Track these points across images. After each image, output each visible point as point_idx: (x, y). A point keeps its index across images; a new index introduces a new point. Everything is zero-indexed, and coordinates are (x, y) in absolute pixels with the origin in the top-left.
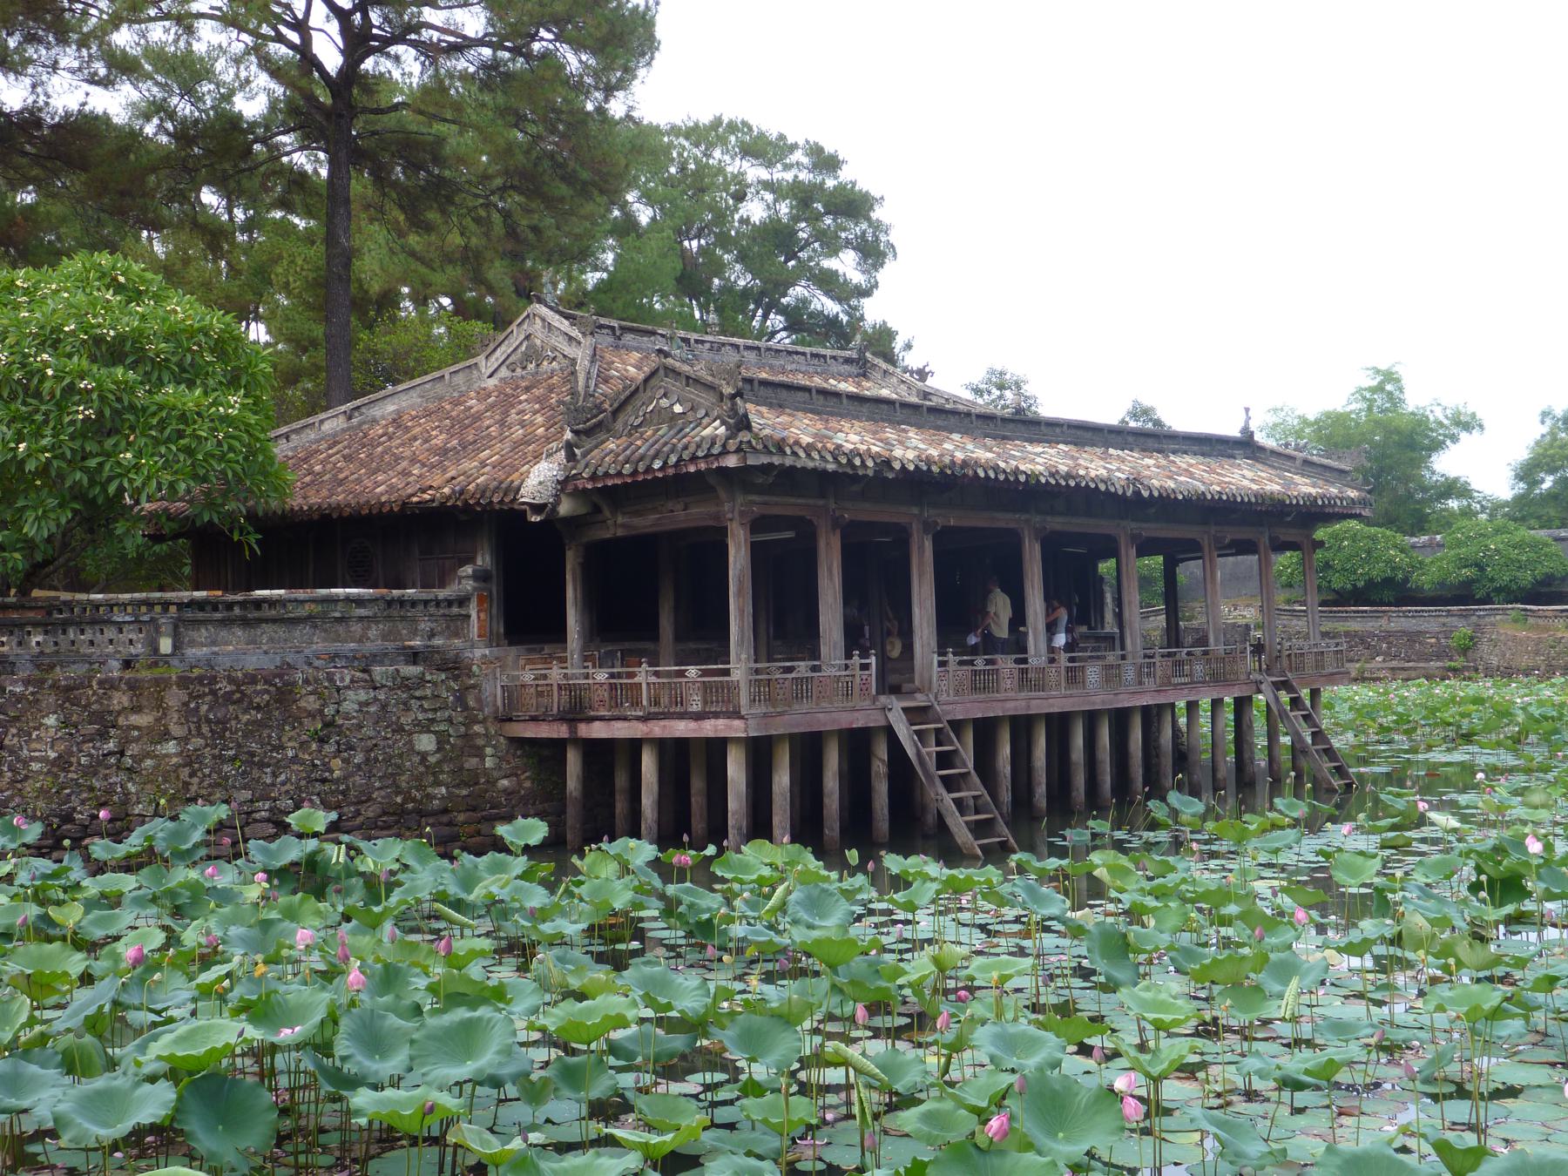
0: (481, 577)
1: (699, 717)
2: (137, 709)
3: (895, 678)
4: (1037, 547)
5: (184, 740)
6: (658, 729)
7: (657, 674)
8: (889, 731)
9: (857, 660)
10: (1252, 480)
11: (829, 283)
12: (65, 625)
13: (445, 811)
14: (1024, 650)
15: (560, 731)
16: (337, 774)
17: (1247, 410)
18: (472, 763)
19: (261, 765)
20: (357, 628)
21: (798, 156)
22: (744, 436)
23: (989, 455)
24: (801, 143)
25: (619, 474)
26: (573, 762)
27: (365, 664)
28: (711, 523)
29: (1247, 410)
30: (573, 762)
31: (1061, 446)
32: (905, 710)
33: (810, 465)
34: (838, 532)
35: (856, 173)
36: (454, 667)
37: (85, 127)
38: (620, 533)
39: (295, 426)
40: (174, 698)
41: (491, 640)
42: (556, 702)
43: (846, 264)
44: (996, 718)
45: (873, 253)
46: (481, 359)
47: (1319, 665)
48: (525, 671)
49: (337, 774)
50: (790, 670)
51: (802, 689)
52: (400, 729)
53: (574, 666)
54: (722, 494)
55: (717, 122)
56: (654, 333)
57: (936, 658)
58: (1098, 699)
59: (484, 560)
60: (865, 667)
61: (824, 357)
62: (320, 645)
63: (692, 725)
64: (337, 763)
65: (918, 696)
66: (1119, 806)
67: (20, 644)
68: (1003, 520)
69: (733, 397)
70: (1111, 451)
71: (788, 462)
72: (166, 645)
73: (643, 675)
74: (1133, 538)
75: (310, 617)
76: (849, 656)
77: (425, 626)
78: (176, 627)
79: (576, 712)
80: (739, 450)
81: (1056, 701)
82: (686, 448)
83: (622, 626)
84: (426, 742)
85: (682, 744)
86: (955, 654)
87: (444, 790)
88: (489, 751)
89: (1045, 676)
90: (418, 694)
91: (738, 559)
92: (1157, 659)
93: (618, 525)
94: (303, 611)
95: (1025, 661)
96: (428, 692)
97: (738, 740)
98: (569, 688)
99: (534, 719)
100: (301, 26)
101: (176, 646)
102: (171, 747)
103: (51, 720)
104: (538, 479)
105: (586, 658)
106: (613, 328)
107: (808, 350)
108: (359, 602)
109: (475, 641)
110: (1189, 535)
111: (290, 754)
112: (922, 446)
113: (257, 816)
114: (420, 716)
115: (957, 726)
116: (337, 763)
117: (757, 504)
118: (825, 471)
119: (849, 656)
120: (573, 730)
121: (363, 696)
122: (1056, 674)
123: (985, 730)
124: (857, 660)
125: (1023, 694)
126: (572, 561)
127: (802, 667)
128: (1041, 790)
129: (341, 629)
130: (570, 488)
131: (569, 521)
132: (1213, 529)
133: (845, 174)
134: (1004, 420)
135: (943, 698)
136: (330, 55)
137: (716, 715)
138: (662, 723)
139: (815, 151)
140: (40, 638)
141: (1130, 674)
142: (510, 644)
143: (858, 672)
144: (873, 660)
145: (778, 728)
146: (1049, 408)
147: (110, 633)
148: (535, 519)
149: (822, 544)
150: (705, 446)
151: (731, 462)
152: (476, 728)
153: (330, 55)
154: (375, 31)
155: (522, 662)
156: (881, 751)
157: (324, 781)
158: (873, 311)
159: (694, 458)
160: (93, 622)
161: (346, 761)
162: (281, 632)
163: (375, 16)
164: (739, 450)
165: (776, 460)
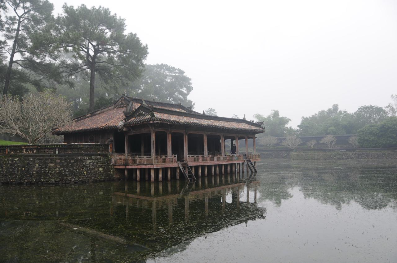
1: (146, 165)
2: (52, 163)
3: (180, 159)
4: (206, 137)
5: (59, 168)
6: (139, 167)
7: (140, 158)
8: (179, 167)
9: (173, 156)
10: (244, 127)
11: (181, 93)
14: (204, 154)
15: (124, 167)
17: (244, 115)
21: (177, 71)
22: (153, 118)
23: (197, 122)
24: (177, 69)
25: (133, 124)
28: (149, 132)
29: (244, 115)
31: (211, 120)
32: (182, 164)
34: (171, 134)
37: (50, 65)
38: (134, 134)
42: (123, 162)
43: (184, 90)
45: (189, 89)
47: (255, 158)
50: (162, 157)
51: (164, 161)
52: (96, 167)
54: (150, 128)
57: (188, 156)
59: (112, 138)
60: (175, 157)
63: (136, 166)
64: (85, 172)
65: (185, 162)
68: (200, 133)
69: (152, 111)
70: (220, 121)
72: (57, 152)
73: (137, 158)
74: (223, 136)
76: (172, 155)
79: (126, 164)
80: (152, 120)
81: (209, 163)
82: (144, 120)
83: (135, 150)
84: (101, 169)
85: (144, 169)
86: (191, 155)
87: (104, 177)
88: (112, 171)
89: (206, 160)
90: (100, 161)
91: (153, 138)
92: (227, 156)
93: (133, 133)
94: (81, 146)
95: (203, 156)
96: (101, 161)
97: (152, 169)
98: (125, 160)
99: (119, 165)
100: (88, 49)
102: (57, 169)
103: (37, 165)
105: (129, 155)
110: (233, 136)
112: (186, 120)
113: (72, 181)
114: (100, 165)
115: (191, 167)
116: (85, 172)
119: (172, 155)
120: (126, 167)
121: (90, 161)
122: (208, 159)
123: (197, 168)
124: (173, 156)
125: (203, 162)
127: (164, 157)
130: (125, 126)
131: (125, 131)
132: (237, 135)
135: (189, 162)
136: (92, 53)
137: (149, 164)
138: (140, 166)
139: (179, 70)
140: (36, 151)
141: (222, 159)
142: (116, 153)
144: (176, 156)
145: (159, 166)
146: (219, 115)
148: (119, 131)
150: (145, 120)
151: (151, 122)
152: (110, 167)
153: (92, 53)
154: (100, 49)
155: (118, 156)
156: (178, 171)
158: (189, 98)
159: (145, 121)
163: (100, 47)
164: (152, 120)
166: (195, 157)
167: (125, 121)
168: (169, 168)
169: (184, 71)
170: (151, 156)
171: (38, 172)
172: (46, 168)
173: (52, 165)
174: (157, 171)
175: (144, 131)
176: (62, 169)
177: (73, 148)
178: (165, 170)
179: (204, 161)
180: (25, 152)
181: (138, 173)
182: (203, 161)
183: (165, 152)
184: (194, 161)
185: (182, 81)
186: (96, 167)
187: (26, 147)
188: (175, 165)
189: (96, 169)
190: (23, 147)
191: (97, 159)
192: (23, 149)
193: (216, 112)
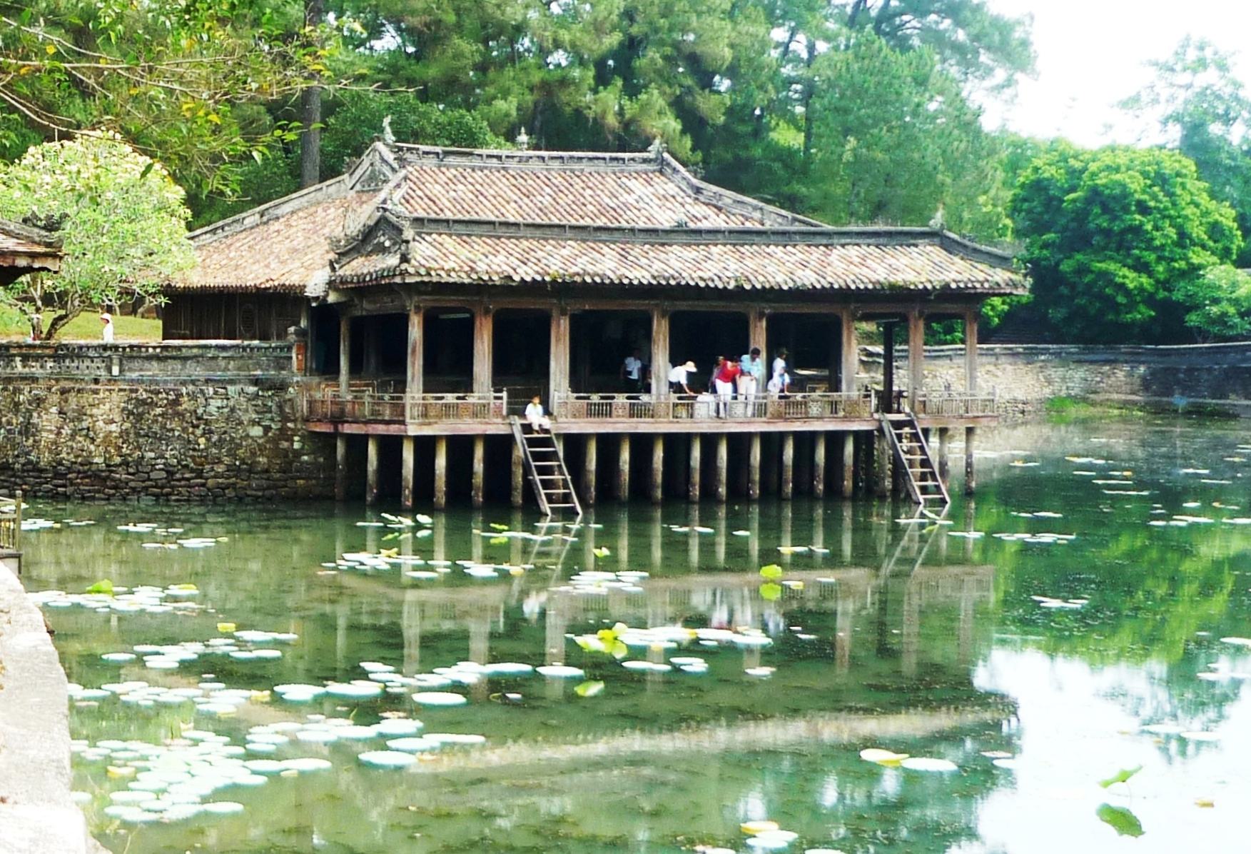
0: (301, 333)
12: (64, 357)
13: (267, 471)
16: (202, 447)
18: (285, 444)
19: (160, 439)
20: (223, 363)
27: (224, 383)
33: (451, 280)
39: (227, 221)
41: (306, 370)
44: (434, 437)
46: (346, 176)
48: (324, 392)
49: (202, 447)
50: (442, 398)
51: (448, 411)
53: (343, 388)
56: (471, 154)
58: (705, 425)
61: (623, 159)
64: (202, 441)
66: (893, 500)
67: (42, 367)
71: (435, 279)
72: (116, 370)
75: (196, 356)
78: (121, 361)
79: (338, 419)
80: (401, 274)
84: (257, 431)
88: (296, 438)
91: (415, 332)
93: (367, 307)
94: (195, 351)
101: (121, 371)
104: (315, 282)
106: (437, 154)
108: (224, 348)
111: (177, 433)
116: (202, 441)
117: (428, 301)
118: (463, 284)
121: (219, 403)
126: (344, 329)
129: (213, 363)
134: (666, 232)
143: (492, 401)
144: (504, 394)
147: (88, 362)
151: (398, 280)
152: (289, 425)
157: (194, 450)
160: (78, 356)
161: (208, 440)
164: (401, 274)
165: (426, 279)
166: (595, 398)
167: (333, 269)
168: (696, 434)
170: (404, 392)
174: (425, 446)
175: (388, 305)
177: (186, 359)
178: (460, 446)
180: (19, 364)
181: (372, 450)
182: (632, 416)
183: (464, 383)
184: (589, 414)
187: (24, 351)
188: (496, 427)
190: (13, 351)
192: (14, 355)
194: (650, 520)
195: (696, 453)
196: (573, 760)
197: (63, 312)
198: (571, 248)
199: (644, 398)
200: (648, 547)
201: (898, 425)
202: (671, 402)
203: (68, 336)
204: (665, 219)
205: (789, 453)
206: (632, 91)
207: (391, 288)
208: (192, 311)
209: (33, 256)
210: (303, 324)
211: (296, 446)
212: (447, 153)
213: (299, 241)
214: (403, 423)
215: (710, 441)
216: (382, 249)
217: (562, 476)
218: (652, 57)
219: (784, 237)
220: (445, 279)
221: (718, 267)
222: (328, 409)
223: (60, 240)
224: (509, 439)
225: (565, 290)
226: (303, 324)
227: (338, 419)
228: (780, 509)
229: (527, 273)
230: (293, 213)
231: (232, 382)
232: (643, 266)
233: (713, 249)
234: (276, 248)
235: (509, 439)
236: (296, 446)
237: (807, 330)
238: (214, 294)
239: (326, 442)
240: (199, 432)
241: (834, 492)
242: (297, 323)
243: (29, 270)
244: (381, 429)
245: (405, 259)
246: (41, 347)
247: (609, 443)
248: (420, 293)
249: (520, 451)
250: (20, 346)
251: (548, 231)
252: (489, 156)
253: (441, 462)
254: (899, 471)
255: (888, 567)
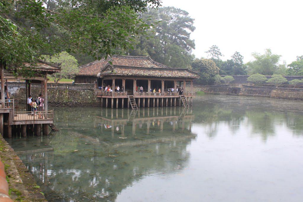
1: (109, 96)
2: (64, 93)
4: (150, 82)
5: (68, 96)
18: (93, 99)
20: (84, 87)
26: (102, 99)
27: (84, 90)
30: (102, 99)
35: (191, 16)
36: (92, 90)
40: (68, 92)
52: (87, 96)
55: (169, 7)
62: (80, 88)
64: (81, 98)
72: (67, 88)
77: (90, 86)
79: (101, 96)
84: (89, 97)
94: (80, 85)
102: (67, 96)
103: (58, 94)
104: (99, 74)
107: (141, 57)
109: (95, 88)
116: (81, 98)
117: (115, 78)
128: (149, 105)
129: (82, 87)
133: (189, 16)
149: (123, 81)
151: (111, 75)
158: (191, 38)
162: (77, 87)
167: (101, 73)
169: (188, 12)
171: (58, 97)
172: (62, 95)
173: (65, 94)
174: (115, 100)
175: (109, 78)
176: (69, 96)
178: (120, 100)
179: (112, 95)
180: (52, 87)
185: (184, 22)
186: (87, 96)
188: (125, 97)
189: (87, 97)
191: (88, 92)
193: (219, 49)
194: (157, 109)
195: (154, 100)
196: (126, 142)
197: (59, 78)
198: (136, 70)
199: (147, 93)
200: (121, 114)
201: (182, 97)
202: (152, 94)
203: (59, 82)
204: (149, 66)
205: (167, 100)
206: (142, 49)
207: (110, 76)
208: (79, 78)
209: (56, 70)
210: (96, 81)
211: (95, 99)
212: (118, 56)
213: (95, 68)
214: (112, 96)
215: (156, 99)
216: (108, 70)
217: (135, 104)
218: (144, 44)
219: (166, 69)
220: (118, 74)
221: (158, 73)
222: (100, 94)
223: (61, 67)
224: (128, 98)
225: (135, 76)
226: (96, 81)
227: (101, 96)
228: (153, 109)
229: (130, 74)
230: (94, 64)
231: (86, 90)
232: (147, 73)
233: (157, 71)
234: (92, 69)
235: (128, 98)
236: (95, 99)
237: (169, 83)
238: (82, 76)
239: (100, 98)
240: (80, 97)
241: (173, 105)
242: (95, 81)
243: (55, 72)
244: (108, 97)
245: (112, 71)
246: (56, 84)
247: (142, 99)
248: (114, 76)
249: (129, 100)
250: (53, 84)
251: (133, 68)
252: (124, 56)
253: (117, 102)
254: (182, 103)
255: (181, 116)
